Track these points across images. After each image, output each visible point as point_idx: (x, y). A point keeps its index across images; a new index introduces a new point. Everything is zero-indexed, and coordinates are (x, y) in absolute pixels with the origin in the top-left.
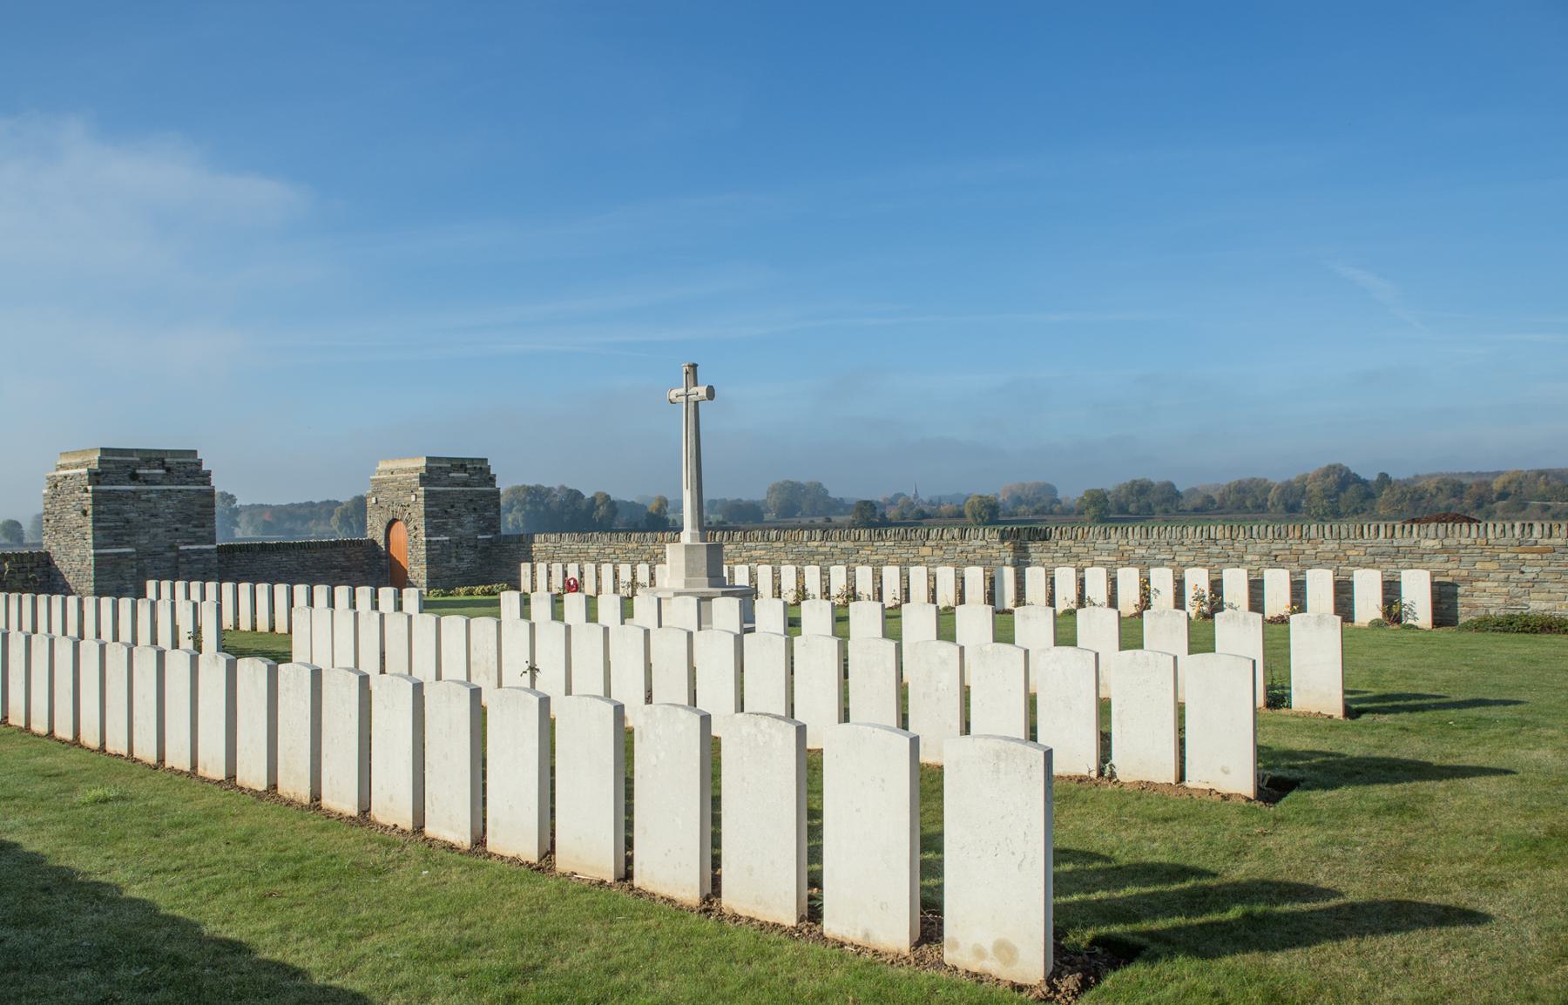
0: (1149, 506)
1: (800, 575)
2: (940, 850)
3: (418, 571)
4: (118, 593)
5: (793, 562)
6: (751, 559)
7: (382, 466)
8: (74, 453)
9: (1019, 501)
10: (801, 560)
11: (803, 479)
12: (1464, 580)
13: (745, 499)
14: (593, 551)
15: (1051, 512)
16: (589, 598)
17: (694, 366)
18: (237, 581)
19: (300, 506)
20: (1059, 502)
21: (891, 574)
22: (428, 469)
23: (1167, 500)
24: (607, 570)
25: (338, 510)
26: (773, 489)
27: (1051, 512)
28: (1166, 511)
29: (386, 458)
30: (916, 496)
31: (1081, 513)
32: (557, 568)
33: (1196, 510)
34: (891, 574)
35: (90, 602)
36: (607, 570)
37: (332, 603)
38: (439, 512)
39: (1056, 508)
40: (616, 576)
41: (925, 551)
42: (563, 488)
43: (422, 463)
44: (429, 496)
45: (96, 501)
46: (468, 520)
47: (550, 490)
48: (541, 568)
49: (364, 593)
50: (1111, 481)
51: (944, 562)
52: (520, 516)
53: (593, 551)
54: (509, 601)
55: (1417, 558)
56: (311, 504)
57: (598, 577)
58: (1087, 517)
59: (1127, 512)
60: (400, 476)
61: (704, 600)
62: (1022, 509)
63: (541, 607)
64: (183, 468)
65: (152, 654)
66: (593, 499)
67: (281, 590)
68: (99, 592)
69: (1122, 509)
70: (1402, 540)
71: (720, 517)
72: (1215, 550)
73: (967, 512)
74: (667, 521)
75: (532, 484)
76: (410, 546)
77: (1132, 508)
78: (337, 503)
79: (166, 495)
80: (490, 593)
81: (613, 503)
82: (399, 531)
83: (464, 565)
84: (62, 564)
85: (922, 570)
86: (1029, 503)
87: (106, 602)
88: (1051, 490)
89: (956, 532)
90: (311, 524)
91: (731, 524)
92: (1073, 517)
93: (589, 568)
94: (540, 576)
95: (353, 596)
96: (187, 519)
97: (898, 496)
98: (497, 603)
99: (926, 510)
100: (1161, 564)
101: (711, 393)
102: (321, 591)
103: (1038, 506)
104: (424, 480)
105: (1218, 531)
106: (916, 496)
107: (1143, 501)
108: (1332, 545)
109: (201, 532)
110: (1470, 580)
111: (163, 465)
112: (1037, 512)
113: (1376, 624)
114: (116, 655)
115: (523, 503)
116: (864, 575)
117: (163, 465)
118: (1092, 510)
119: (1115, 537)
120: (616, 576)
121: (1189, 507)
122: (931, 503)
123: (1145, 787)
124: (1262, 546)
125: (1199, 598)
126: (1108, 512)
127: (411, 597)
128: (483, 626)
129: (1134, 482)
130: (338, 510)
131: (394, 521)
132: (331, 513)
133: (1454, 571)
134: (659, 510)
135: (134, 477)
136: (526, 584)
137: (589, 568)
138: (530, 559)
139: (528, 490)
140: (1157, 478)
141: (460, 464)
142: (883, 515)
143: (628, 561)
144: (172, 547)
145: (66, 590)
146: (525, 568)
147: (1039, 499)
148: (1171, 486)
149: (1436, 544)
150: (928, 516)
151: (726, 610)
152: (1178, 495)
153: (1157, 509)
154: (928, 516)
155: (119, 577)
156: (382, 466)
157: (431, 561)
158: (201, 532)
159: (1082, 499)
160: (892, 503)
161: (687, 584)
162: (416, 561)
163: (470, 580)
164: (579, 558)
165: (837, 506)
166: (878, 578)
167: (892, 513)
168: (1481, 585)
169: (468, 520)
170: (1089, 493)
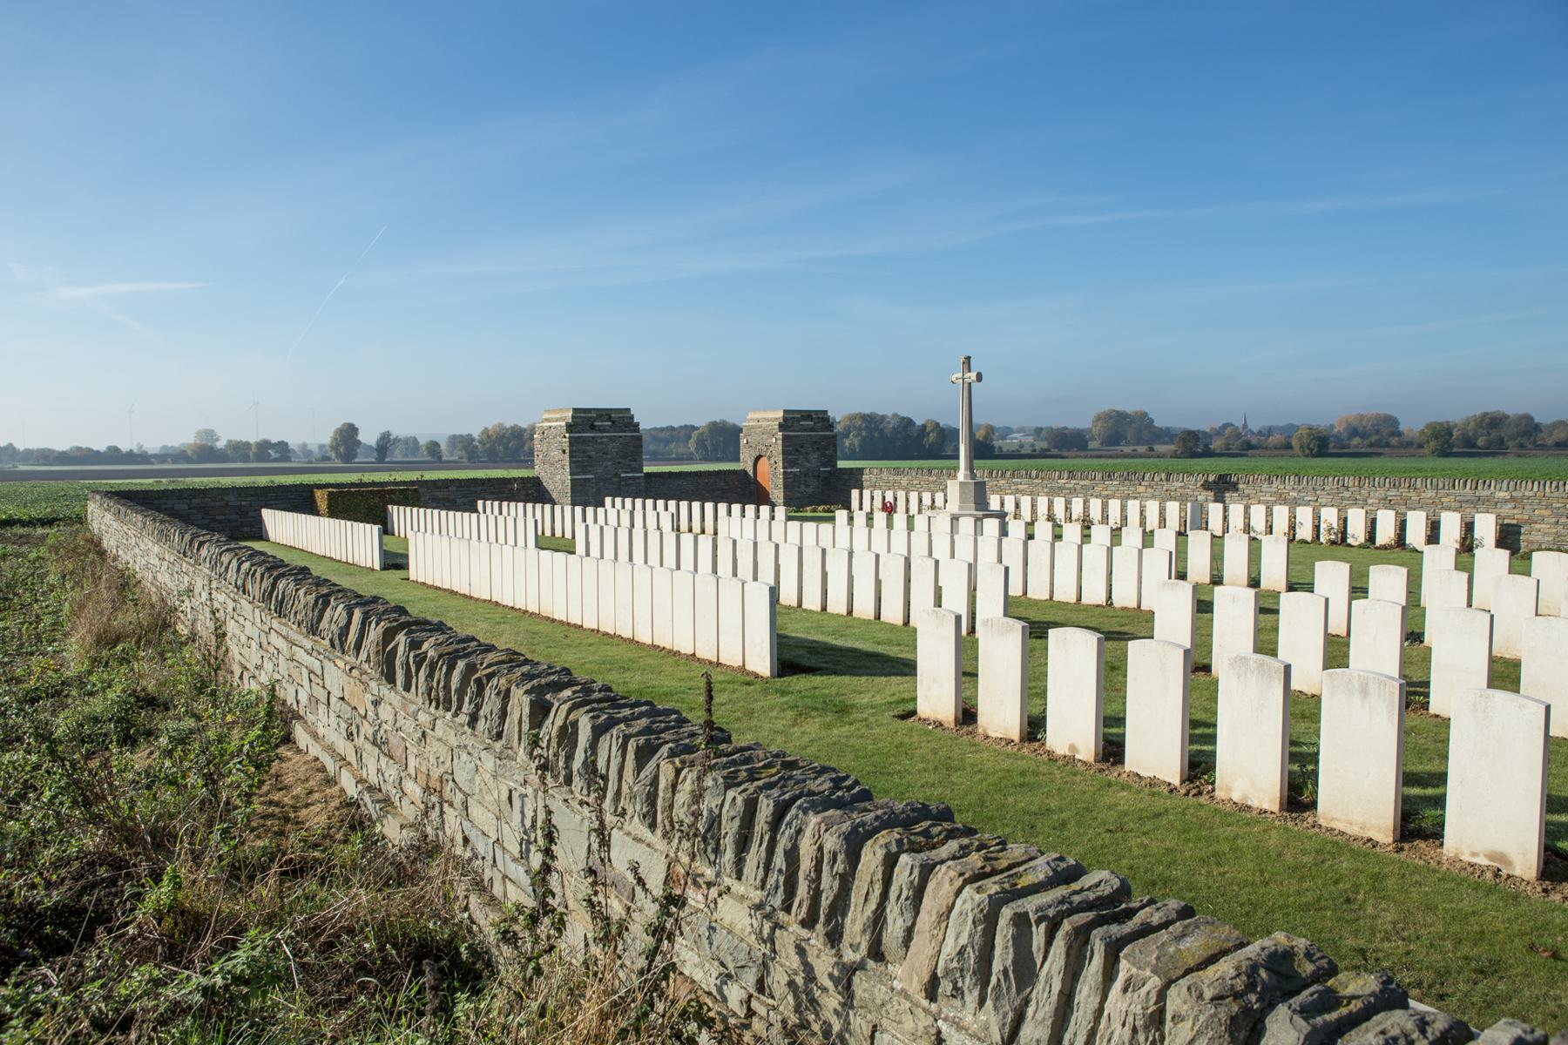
0: (1501, 441)
1: (1051, 504)
2: (1212, 739)
3: (777, 494)
4: (585, 505)
5: (1047, 494)
6: (1018, 491)
7: (751, 415)
8: (554, 411)
9: (1354, 432)
10: (1052, 493)
11: (1130, 408)
12: (1526, 522)
13: (1071, 426)
14: (904, 482)
15: (1388, 445)
16: (1027, 524)
17: (968, 358)
18: (691, 501)
19: (662, 430)
20: (1400, 434)
21: (1115, 505)
22: (785, 419)
23: (1524, 434)
24: (914, 496)
25: (695, 434)
26: (1098, 418)
27: (1388, 445)
28: (1522, 446)
29: (755, 410)
30: (1245, 426)
31: (1420, 446)
32: (878, 494)
33: (1558, 445)
34: (1115, 505)
35: (568, 509)
36: (914, 496)
37: (729, 513)
38: (792, 450)
39: (1394, 441)
40: (920, 501)
41: (1141, 489)
42: (895, 415)
43: (781, 414)
44: (785, 438)
45: (571, 444)
46: (814, 456)
47: (883, 417)
48: (866, 493)
49: (649, 502)
50: (1459, 410)
51: (1153, 497)
52: (856, 441)
53: (904, 482)
54: (841, 515)
55: (1488, 504)
56: (672, 429)
57: (908, 501)
58: (1426, 450)
59: (1474, 445)
60: (764, 424)
61: (978, 520)
62: (1356, 441)
63: (860, 518)
64: (621, 420)
65: (690, 537)
66: (924, 426)
67: (709, 506)
68: (574, 504)
69: (1469, 443)
70: (1483, 492)
71: (1045, 445)
72: (1347, 494)
73: (1294, 442)
74: (993, 447)
75: (867, 411)
76: (772, 475)
77: (1481, 442)
78: (694, 428)
79: (612, 439)
80: (829, 511)
81: (943, 430)
82: (763, 465)
83: (810, 490)
84: (548, 484)
85: (1137, 502)
86: (1363, 436)
87: (578, 509)
88: (1391, 422)
89: (1163, 476)
90: (673, 445)
91: (1055, 451)
92: (1412, 450)
93: (901, 495)
94: (865, 499)
95: (743, 511)
96: (625, 456)
97: (1226, 426)
98: (833, 519)
99: (1254, 441)
100: (1307, 504)
101: (979, 377)
102: (736, 508)
103: (1373, 439)
104: (782, 427)
105: (1350, 481)
106: (1245, 426)
107: (1494, 434)
108: (1430, 493)
109: (634, 464)
110: (1530, 522)
111: (610, 419)
112: (1371, 445)
113: (1361, 546)
114: (654, 537)
115: (860, 429)
116: (1095, 506)
117: (610, 419)
118: (1432, 444)
119: (1276, 483)
120: (920, 501)
121: (1550, 442)
122: (1260, 433)
123: (1125, 609)
124: (1380, 493)
125: (1330, 530)
126: (1451, 446)
127: (780, 512)
128: (826, 528)
129: (1485, 414)
130: (695, 434)
131: (758, 458)
132: (689, 437)
133: (1514, 515)
134: (985, 437)
135: (593, 427)
136: (855, 504)
137: (901, 495)
138: (847, 506)
139: (864, 417)
140: (1513, 409)
141: (808, 415)
142: (1206, 446)
143: (929, 490)
144: (617, 475)
145: (553, 503)
146: (855, 493)
147: (1377, 432)
148: (1528, 418)
149: (1506, 495)
150: (1255, 448)
151: (991, 525)
152: (1537, 428)
153: (1511, 443)
154: (1255, 448)
155: (587, 494)
156: (751, 415)
157: (786, 486)
158: (634, 464)
159: (1422, 432)
160: (1219, 433)
161: (960, 508)
162: (776, 487)
163: (815, 500)
164: (894, 486)
165: (1165, 435)
166: (1105, 508)
167: (1216, 445)
168: (1538, 526)
169: (814, 456)
170: (1429, 426)
